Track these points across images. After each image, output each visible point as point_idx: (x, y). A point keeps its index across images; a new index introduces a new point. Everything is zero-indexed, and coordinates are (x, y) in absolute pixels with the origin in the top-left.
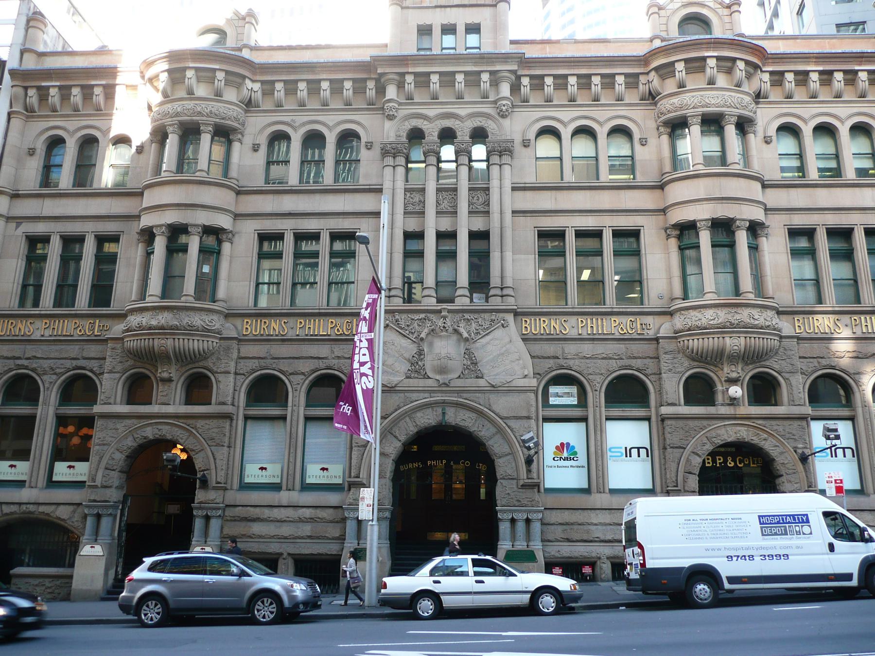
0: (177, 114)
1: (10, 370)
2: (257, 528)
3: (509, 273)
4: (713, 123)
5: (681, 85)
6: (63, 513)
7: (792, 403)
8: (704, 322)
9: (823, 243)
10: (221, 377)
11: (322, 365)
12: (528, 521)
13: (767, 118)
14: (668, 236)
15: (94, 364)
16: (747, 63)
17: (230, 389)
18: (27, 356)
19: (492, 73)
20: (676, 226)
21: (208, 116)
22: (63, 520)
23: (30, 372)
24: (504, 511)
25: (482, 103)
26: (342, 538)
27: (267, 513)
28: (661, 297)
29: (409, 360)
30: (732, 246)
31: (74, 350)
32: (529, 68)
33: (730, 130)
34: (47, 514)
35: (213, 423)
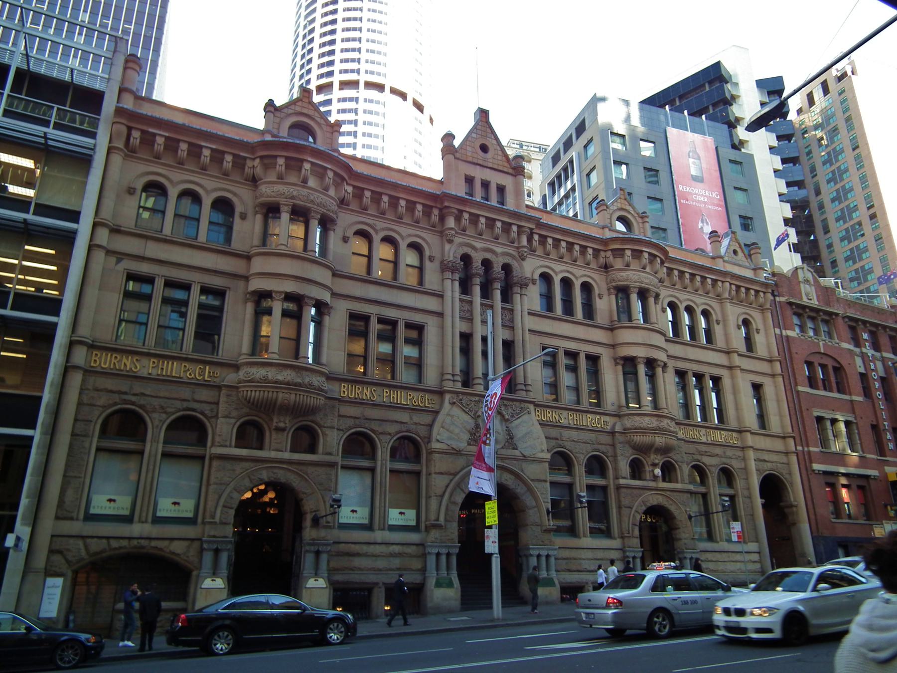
0: (293, 198)
1: (115, 404)
2: (357, 562)
3: (529, 375)
4: (300, 214)
5: (280, 177)
6: (178, 547)
7: (683, 482)
8: (644, 425)
9: (375, 327)
10: (328, 431)
11: (404, 429)
12: (548, 556)
13: (346, 221)
14: (616, 364)
15: (206, 408)
16: (335, 173)
17: (332, 440)
18: (134, 391)
19: (519, 227)
20: (254, 293)
21: (318, 205)
22: (178, 555)
23: (137, 409)
24: (534, 549)
25: (509, 246)
26: (424, 570)
27: (365, 548)
28: (613, 404)
29: (469, 431)
30: (636, 374)
31: (186, 393)
32: (540, 229)
33: (634, 297)
34: (161, 549)
35: (321, 470)
